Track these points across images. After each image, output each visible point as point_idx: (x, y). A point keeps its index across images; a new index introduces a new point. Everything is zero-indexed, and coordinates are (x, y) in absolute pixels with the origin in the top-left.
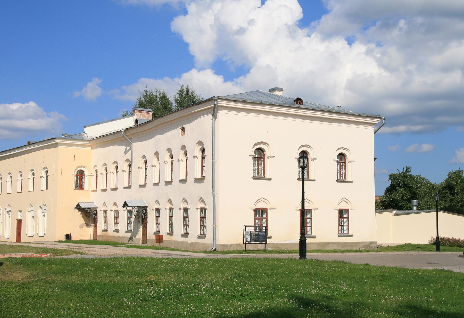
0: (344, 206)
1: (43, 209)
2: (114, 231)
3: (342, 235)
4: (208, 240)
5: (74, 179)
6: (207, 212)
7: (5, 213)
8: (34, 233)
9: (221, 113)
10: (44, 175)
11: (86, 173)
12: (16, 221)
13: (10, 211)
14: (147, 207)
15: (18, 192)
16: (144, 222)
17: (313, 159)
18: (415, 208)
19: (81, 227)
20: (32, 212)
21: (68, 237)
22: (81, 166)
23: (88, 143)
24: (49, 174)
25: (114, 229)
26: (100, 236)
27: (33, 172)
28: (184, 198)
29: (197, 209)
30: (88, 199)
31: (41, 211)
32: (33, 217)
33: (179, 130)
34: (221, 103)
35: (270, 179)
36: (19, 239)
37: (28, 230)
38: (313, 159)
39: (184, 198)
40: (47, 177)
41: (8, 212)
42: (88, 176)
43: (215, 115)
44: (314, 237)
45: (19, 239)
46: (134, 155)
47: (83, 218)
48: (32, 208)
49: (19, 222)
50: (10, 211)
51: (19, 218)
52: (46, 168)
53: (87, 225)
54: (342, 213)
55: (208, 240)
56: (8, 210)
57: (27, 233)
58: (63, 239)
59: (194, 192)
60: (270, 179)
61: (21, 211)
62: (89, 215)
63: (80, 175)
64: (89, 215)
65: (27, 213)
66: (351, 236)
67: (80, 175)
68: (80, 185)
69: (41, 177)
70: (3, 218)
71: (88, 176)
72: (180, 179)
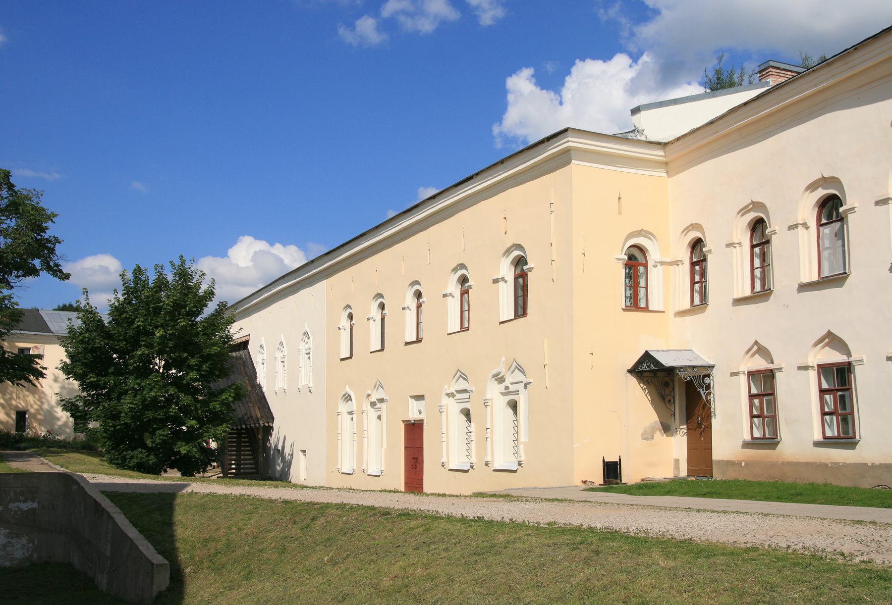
1: (507, 383)
2: (817, 444)
5: (622, 272)
7: (366, 406)
8: (474, 459)
10: (376, 314)
11: (654, 254)
12: (402, 426)
13: (381, 400)
14: (713, 367)
15: (407, 344)
16: (699, 410)
19: (648, 436)
20: (458, 396)
21: (612, 470)
22: (639, 233)
23: (657, 154)
24: (386, 311)
25: (818, 436)
26: (729, 463)
27: (417, 287)
28: (756, 343)
29: (806, 368)
30: (679, 342)
31: (501, 388)
32: (467, 414)
36: (414, 479)
37: (447, 449)
39: (756, 343)
40: (383, 319)
41: (373, 404)
42: (662, 263)
45: (414, 479)
47: (653, 402)
48: (462, 384)
49: (414, 430)
50: (381, 400)
51: (413, 416)
52: (350, 307)
53: (667, 429)
56: (374, 399)
57: (444, 460)
58: (598, 478)
61: (420, 398)
62: (679, 392)
63: (635, 263)
64: (679, 392)
65: (445, 401)
67: (635, 263)
68: (635, 301)
69: (445, 296)
70: (360, 421)
71: (662, 263)
72: (736, 297)
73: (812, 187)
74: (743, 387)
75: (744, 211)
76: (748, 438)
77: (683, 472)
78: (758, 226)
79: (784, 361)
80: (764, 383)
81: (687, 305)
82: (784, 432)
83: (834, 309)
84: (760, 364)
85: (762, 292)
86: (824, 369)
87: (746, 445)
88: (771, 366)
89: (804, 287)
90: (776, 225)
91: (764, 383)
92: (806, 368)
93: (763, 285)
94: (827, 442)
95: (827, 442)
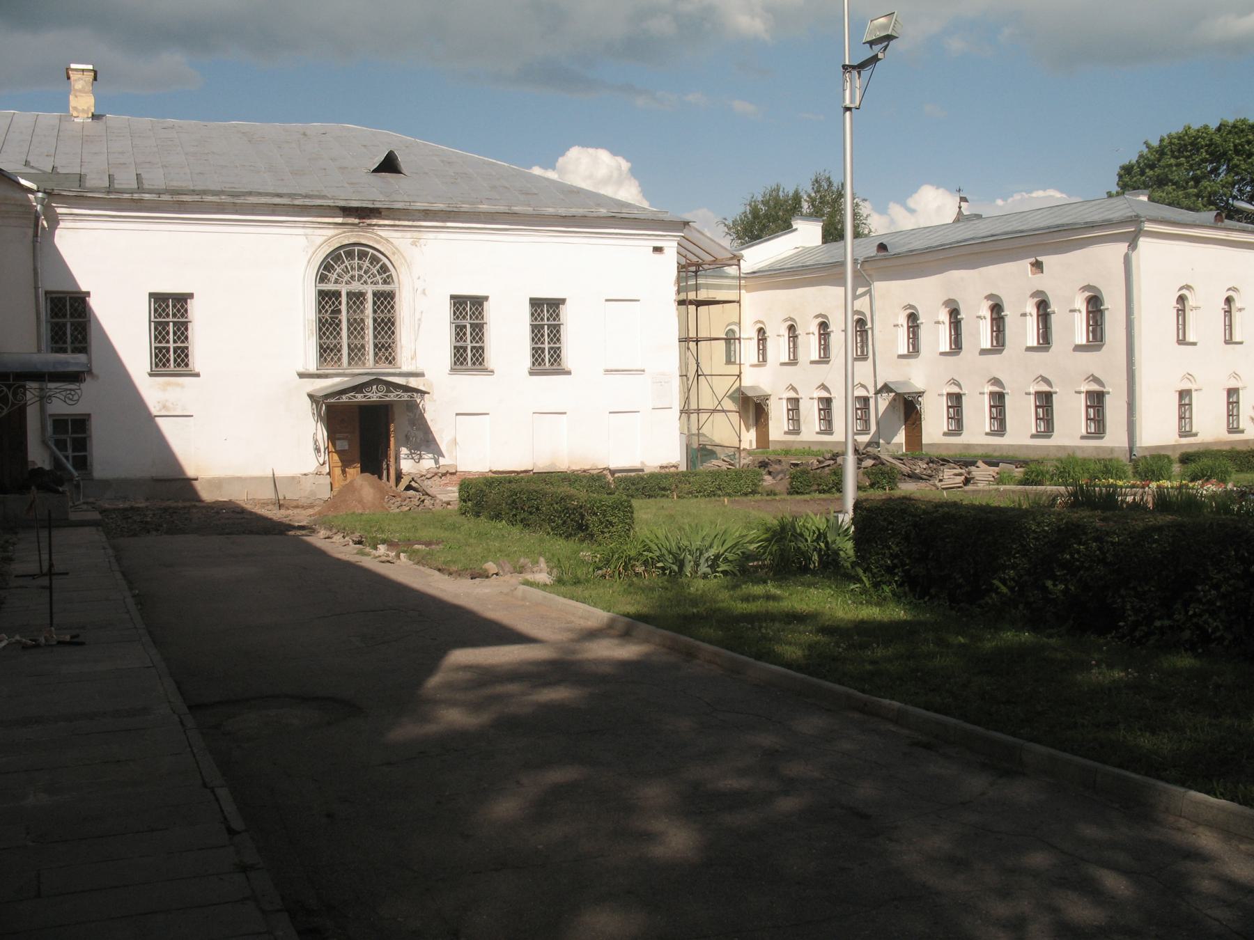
0: (1233, 384)
2: (1083, 437)
3: (1231, 430)
4: (1115, 438)
6: (1108, 400)
9: (1143, 242)
17: (1240, 310)
18: (69, 346)
25: (818, 429)
29: (1079, 393)
30: (755, 379)
33: (1026, 264)
34: (1148, 227)
35: (1194, 344)
38: (1240, 310)
43: (1133, 245)
44: (1242, 432)
46: (877, 304)
54: (1184, 394)
55: (1115, 438)
59: (335, 342)
60: (1194, 344)
66: (1196, 435)
73: (817, 317)
74: (784, 405)
75: (786, 320)
76: (1034, 431)
77: (754, 446)
78: (792, 328)
79: (803, 394)
80: (794, 404)
81: (817, 358)
82: (803, 428)
83: (996, 365)
84: (792, 395)
85: (793, 362)
86: (1038, 394)
87: (786, 433)
88: (1101, 389)
89: (813, 362)
90: (800, 331)
91: (794, 404)
92: (1079, 393)
93: (862, 352)
94: (821, 432)
95: (821, 432)
